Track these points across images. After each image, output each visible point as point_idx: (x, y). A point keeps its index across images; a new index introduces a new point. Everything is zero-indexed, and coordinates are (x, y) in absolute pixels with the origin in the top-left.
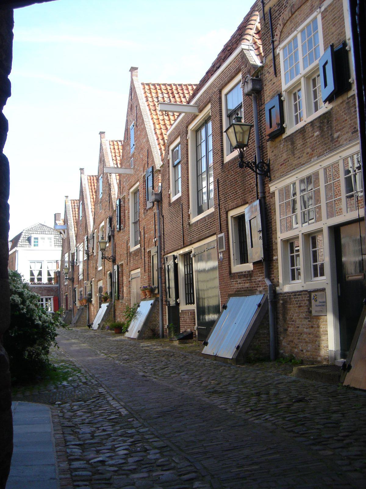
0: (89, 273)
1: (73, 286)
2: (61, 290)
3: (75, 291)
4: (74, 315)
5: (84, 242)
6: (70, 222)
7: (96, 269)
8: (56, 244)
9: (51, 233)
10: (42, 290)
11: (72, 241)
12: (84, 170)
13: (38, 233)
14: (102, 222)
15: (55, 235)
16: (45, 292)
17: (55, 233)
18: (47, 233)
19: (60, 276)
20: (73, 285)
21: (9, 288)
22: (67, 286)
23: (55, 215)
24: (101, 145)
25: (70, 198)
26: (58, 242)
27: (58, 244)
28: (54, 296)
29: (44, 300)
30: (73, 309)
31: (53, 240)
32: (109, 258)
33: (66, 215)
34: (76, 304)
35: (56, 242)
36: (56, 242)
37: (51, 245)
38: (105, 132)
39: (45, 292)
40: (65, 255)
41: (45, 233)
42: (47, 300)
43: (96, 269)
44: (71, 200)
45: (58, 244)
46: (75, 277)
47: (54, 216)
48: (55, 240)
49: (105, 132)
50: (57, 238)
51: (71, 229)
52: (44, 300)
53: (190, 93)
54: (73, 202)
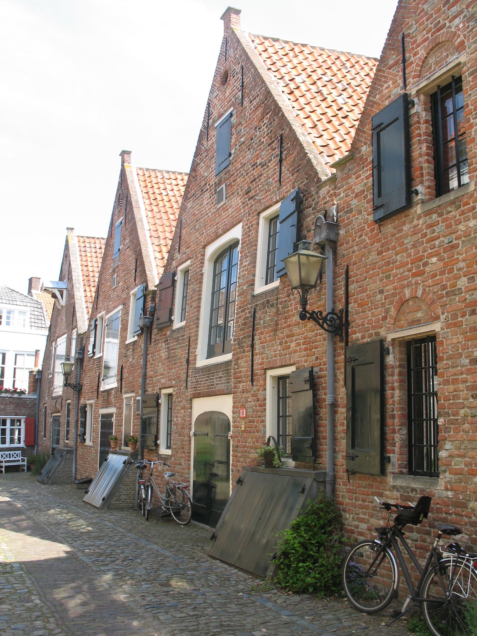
0: (150, 373)
1: (79, 402)
2: (41, 405)
3: (86, 412)
4: (76, 461)
5: (125, 304)
6: (76, 274)
7: (188, 361)
8: (33, 324)
9: (25, 304)
10: (6, 404)
11: (80, 310)
12: (132, 154)
13: (4, 301)
14: (234, 226)
15: (32, 309)
16: (10, 408)
17: (32, 305)
18: (18, 303)
19: (41, 380)
20: (79, 399)
21: (448, 185)
22: (60, 400)
23: (31, 280)
24: (67, 241)
25: (76, 233)
26: (36, 321)
27: (36, 325)
28: (28, 415)
29: (8, 422)
30: (76, 450)
31: (28, 315)
32: (325, 319)
33: (66, 268)
34: (85, 440)
35: (33, 320)
36: (33, 320)
37: (24, 325)
38: (130, 152)
39: (10, 408)
40: (58, 340)
41: (15, 303)
42: (13, 422)
43: (188, 361)
44: (78, 236)
45: (36, 325)
46: (86, 382)
47: (28, 281)
48: (33, 317)
49: (130, 152)
50: (36, 313)
51: (79, 288)
52: (8, 422)
53: (181, 191)
54: (140, 172)
